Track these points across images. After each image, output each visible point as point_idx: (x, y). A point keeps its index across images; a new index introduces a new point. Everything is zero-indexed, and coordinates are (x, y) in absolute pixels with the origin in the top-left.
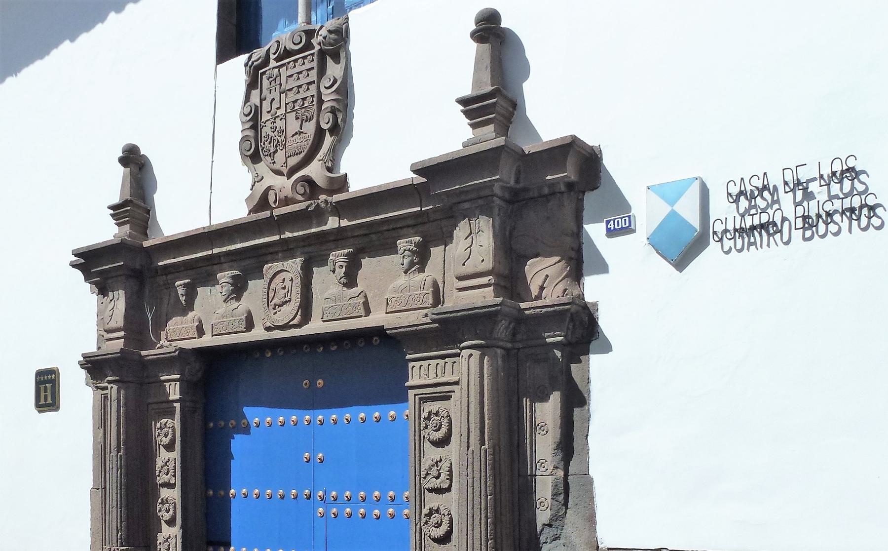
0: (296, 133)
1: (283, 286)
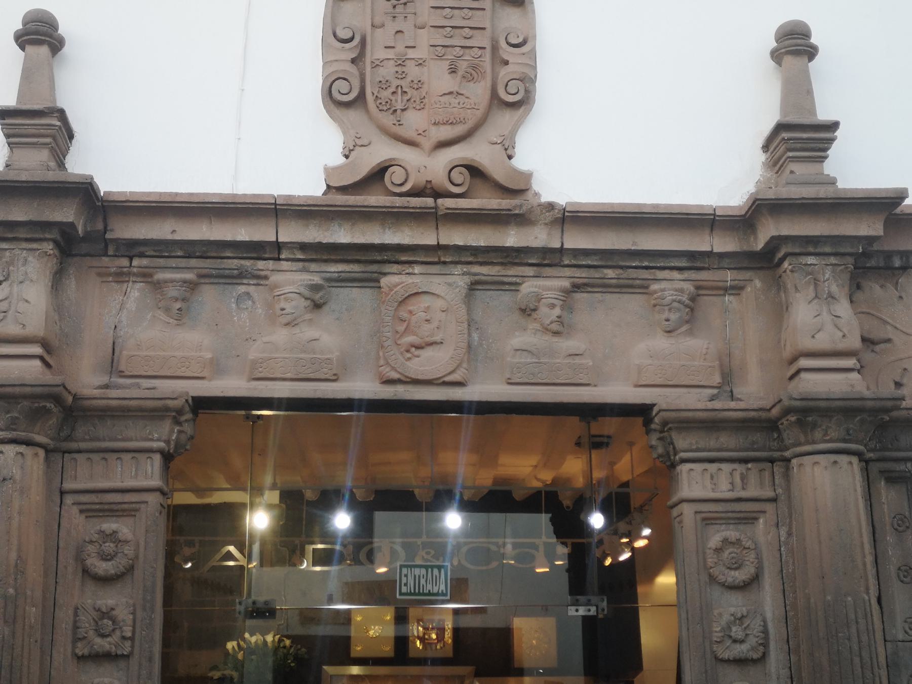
0: (451, 93)
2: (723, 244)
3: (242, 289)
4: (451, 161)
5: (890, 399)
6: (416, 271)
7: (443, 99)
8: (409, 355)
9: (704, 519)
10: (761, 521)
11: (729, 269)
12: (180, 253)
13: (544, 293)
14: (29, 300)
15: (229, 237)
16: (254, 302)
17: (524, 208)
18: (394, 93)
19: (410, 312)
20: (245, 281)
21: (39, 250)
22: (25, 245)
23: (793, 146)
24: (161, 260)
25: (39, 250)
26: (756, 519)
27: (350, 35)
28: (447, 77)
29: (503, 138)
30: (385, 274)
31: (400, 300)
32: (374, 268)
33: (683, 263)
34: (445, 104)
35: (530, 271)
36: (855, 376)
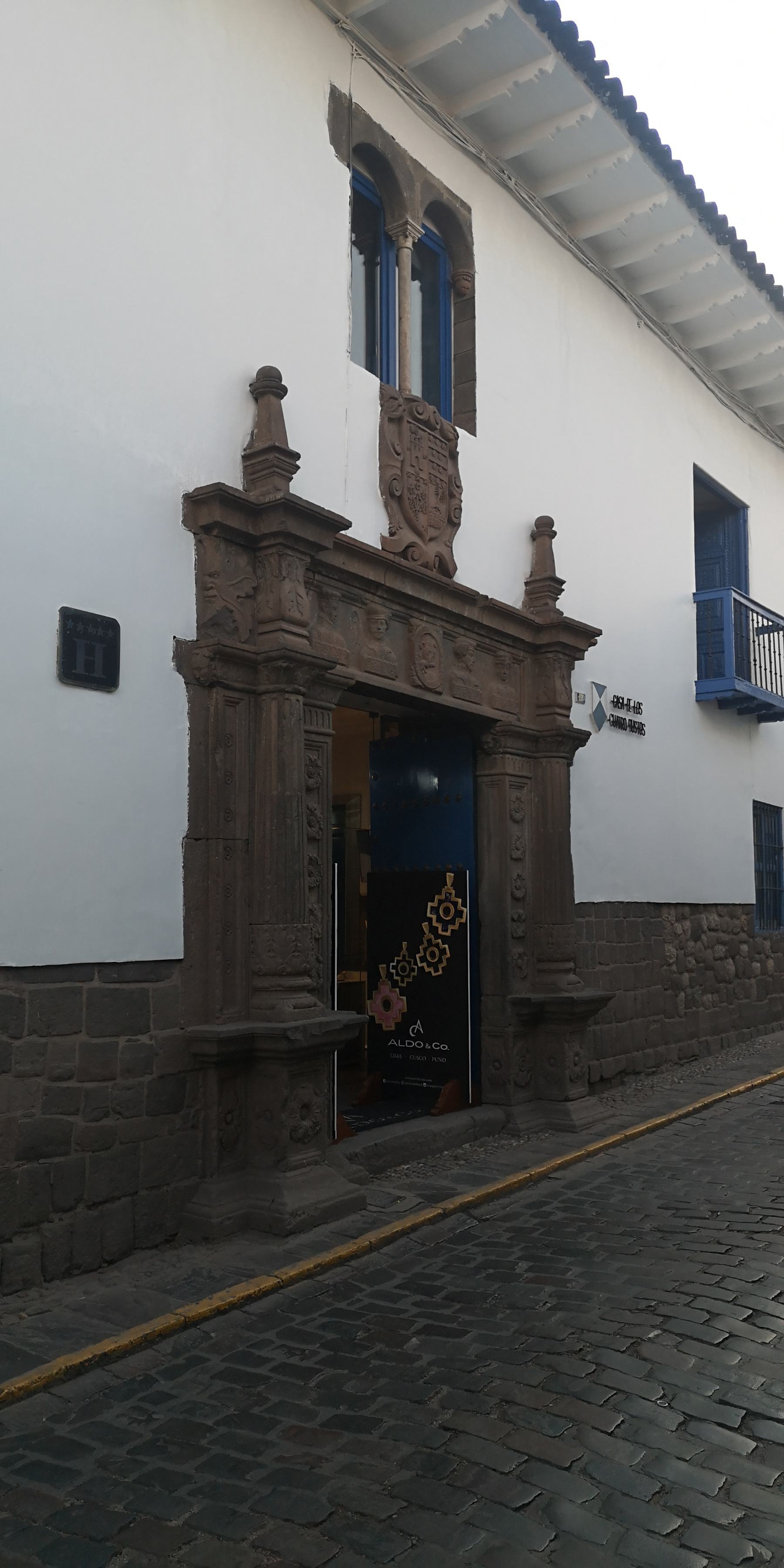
2: (527, 636)
3: (354, 609)
5: (310, 656)
6: (424, 619)
9: (226, 701)
10: (526, 788)
11: (523, 651)
12: (336, 577)
15: (361, 573)
16: (358, 619)
20: (357, 604)
21: (304, 560)
22: (299, 555)
23: (552, 590)
24: (327, 579)
25: (304, 560)
26: (523, 787)
30: (412, 617)
32: (409, 612)
33: (509, 642)
35: (462, 631)
36: (305, 641)
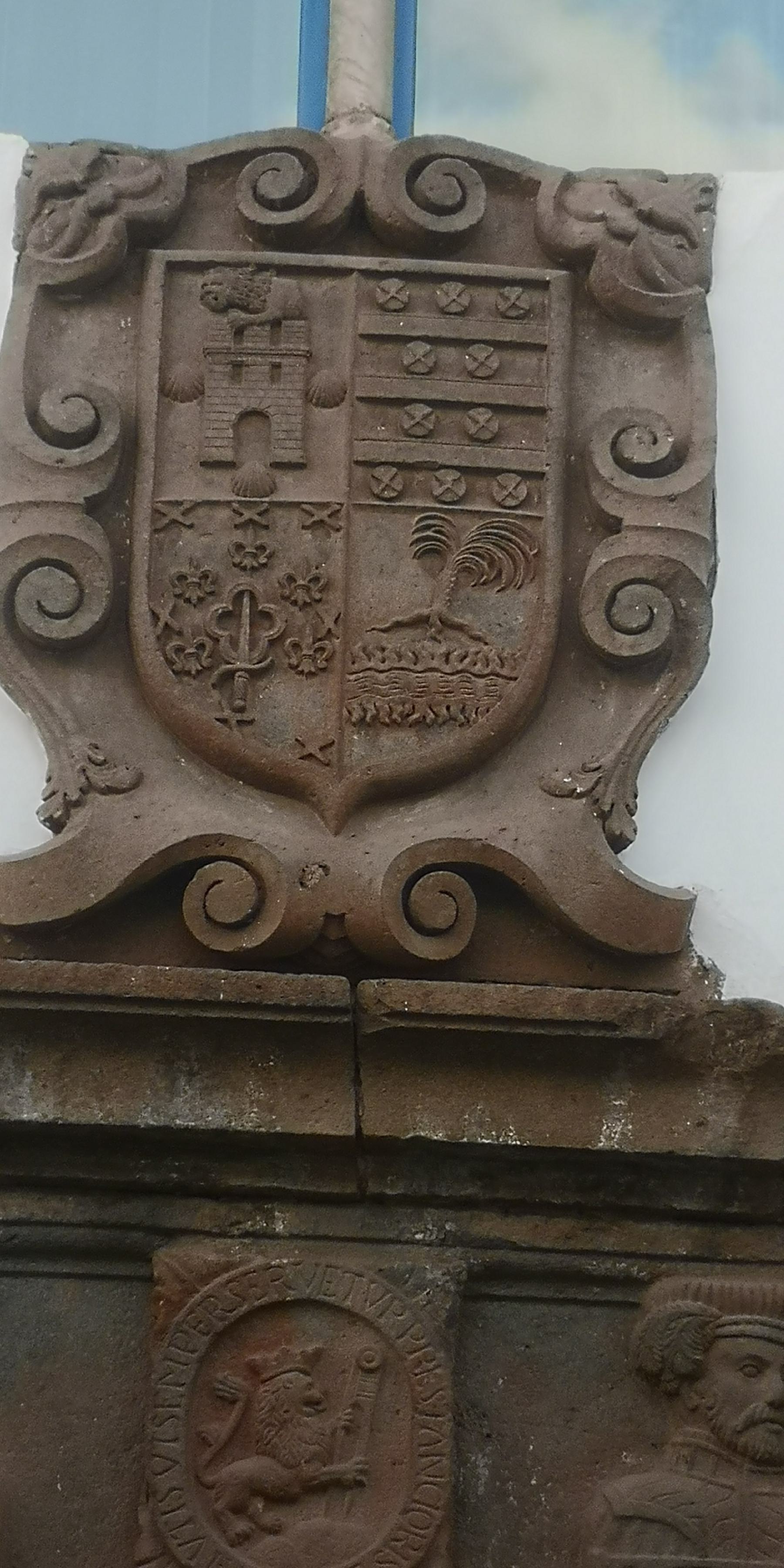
0: (421, 622)
1: (315, 1393)
4: (413, 852)
7: (391, 642)
8: (241, 1526)
13: (726, 1318)
14: (216, 879)
17: (662, 1019)
18: (225, 616)
19: (254, 1371)
27: (86, 418)
28: (411, 567)
29: (596, 775)
31: (220, 1325)
34: (400, 657)
